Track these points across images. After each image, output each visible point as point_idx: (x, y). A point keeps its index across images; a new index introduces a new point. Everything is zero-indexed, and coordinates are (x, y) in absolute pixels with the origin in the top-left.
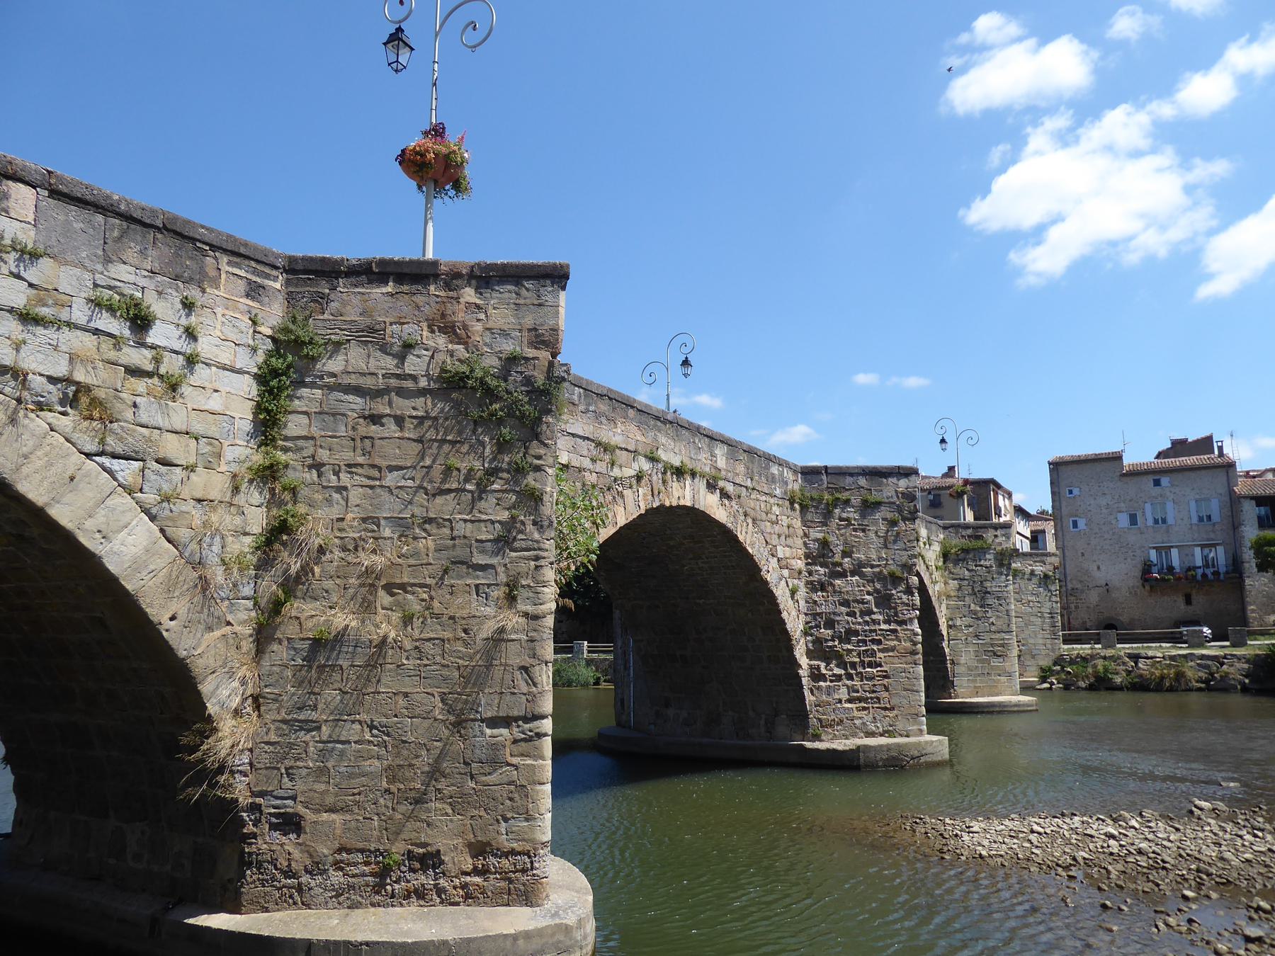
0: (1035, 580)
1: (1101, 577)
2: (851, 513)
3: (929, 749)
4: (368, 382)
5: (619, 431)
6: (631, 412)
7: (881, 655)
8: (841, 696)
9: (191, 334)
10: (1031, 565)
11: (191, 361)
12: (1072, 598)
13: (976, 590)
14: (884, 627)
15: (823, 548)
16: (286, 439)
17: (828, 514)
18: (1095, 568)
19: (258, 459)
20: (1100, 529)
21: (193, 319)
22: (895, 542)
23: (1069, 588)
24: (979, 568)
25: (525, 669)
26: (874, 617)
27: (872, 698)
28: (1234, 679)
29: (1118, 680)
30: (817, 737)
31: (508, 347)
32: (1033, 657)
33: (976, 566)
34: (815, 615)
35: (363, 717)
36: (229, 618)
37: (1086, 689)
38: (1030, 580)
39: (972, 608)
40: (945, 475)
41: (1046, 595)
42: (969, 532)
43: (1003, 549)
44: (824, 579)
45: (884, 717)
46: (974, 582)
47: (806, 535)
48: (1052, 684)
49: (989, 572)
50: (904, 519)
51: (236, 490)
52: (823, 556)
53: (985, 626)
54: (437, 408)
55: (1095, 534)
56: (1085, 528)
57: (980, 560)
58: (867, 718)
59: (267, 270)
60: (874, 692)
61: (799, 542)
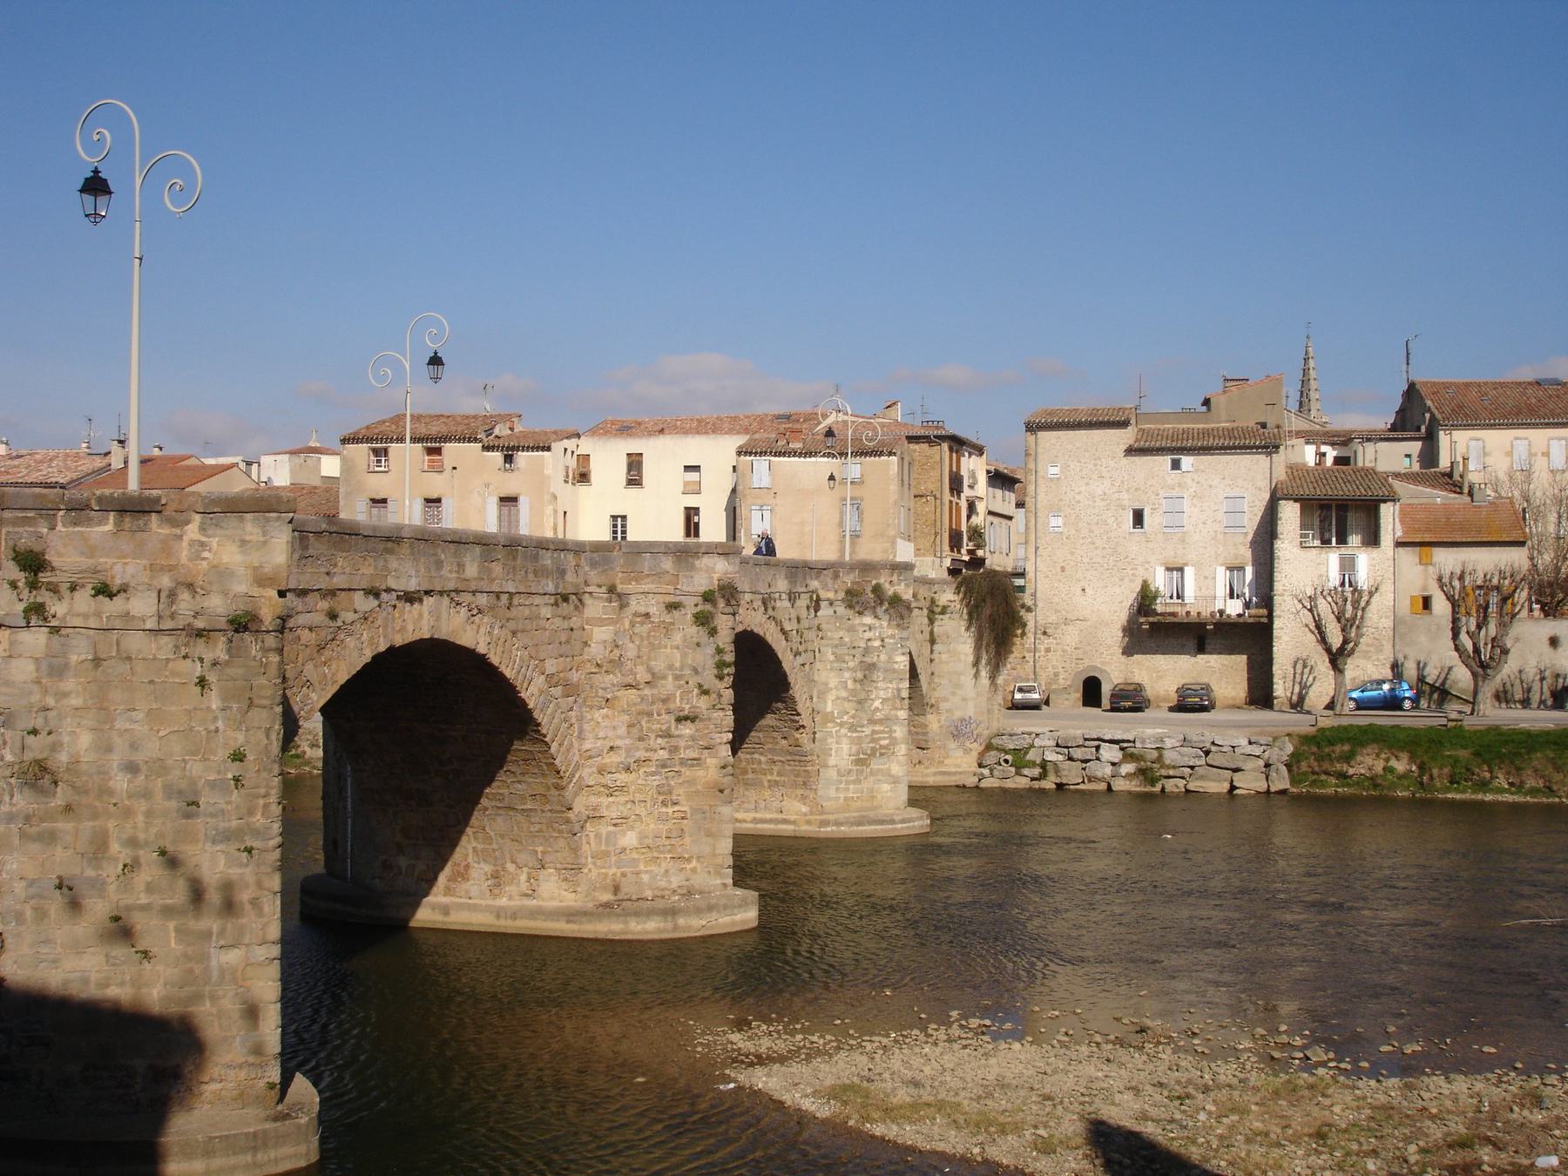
18: (1079, 591)
20: (1091, 531)
55: (1083, 538)
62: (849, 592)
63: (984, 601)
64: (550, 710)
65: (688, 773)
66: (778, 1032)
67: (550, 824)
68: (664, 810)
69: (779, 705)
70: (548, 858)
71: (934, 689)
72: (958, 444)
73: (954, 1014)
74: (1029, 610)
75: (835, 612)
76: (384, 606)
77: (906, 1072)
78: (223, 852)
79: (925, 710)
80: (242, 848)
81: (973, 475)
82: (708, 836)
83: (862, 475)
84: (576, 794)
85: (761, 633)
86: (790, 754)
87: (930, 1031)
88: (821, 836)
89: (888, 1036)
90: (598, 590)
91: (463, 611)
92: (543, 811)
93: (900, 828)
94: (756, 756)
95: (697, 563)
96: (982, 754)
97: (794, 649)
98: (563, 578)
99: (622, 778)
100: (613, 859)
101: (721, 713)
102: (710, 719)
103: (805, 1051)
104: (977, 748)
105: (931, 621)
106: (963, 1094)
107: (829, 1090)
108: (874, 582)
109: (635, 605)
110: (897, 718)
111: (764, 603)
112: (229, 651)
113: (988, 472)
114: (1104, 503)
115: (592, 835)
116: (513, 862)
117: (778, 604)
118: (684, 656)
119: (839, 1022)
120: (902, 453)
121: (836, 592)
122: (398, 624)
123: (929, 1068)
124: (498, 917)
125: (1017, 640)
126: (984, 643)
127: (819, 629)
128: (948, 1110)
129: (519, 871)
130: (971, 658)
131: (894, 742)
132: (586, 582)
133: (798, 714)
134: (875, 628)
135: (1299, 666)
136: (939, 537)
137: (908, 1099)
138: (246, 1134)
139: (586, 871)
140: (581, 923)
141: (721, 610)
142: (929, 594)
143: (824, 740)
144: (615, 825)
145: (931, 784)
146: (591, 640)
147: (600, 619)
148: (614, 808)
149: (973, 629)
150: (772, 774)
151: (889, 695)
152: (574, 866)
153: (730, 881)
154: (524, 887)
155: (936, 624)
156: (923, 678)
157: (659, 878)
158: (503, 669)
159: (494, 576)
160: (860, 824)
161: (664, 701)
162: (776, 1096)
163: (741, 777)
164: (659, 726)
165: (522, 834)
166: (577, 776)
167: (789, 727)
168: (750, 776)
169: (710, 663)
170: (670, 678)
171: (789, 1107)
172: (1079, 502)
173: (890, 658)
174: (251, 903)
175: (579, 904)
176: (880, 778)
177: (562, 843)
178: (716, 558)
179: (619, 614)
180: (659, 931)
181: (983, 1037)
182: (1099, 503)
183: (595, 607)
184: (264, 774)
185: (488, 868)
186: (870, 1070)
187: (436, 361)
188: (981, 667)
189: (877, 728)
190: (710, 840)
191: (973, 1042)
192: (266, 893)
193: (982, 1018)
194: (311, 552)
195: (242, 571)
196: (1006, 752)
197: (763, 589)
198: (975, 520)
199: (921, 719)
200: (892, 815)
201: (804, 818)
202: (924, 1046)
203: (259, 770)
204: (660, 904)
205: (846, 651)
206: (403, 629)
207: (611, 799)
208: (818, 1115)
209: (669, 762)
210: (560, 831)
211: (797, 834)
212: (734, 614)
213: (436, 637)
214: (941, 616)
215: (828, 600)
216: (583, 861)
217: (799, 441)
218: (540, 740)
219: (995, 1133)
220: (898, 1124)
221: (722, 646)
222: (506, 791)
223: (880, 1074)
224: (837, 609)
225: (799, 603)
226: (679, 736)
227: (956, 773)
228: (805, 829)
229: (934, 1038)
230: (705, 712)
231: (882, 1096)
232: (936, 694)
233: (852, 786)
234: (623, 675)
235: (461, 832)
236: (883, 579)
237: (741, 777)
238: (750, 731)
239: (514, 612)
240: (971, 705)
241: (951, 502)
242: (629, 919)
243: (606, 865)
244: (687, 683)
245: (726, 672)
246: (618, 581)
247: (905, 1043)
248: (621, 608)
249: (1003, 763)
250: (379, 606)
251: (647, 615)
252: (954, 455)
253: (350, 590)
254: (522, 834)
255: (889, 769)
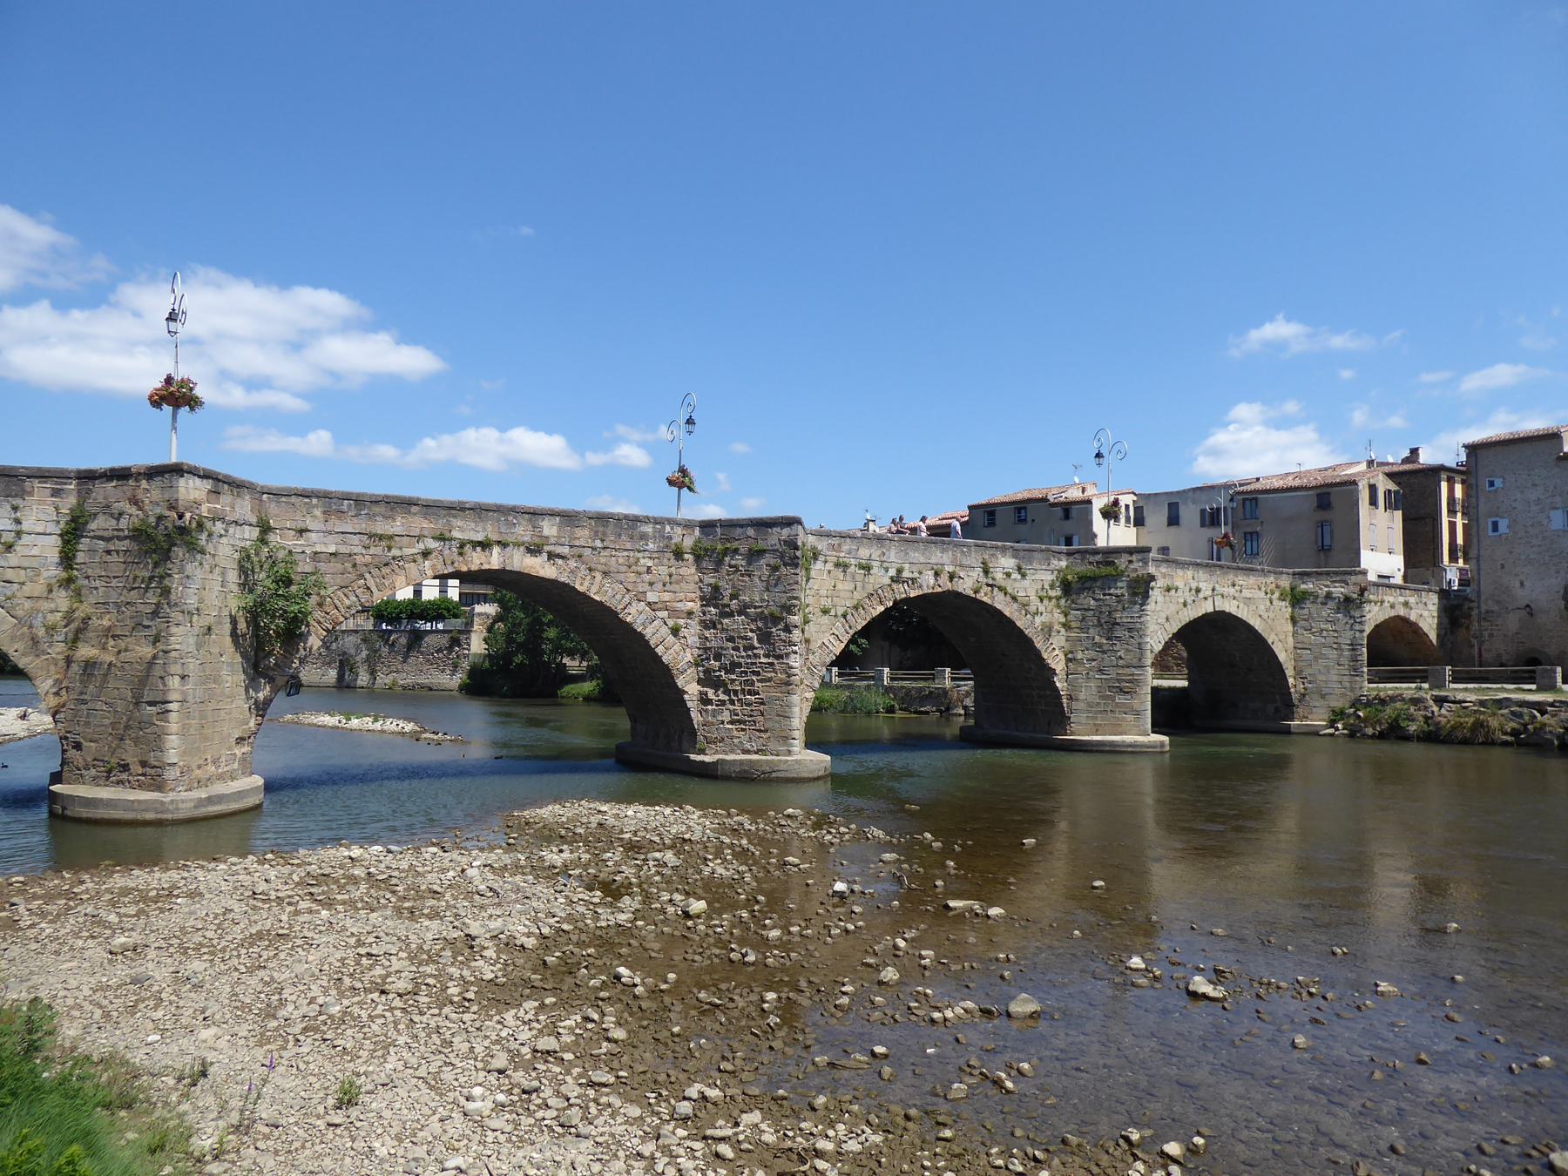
0: (1331, 604)
1: (1523, 596)
2: (739, 561)
3: (783, 767)
4: (105, 534)
5: (399, 524)
6: (414, 509)
7: (760, 685)
8: (724, 719)
9: (18, 522)
10: (1326, 586)
11: (19, 534)
12: (1486, 624)
13: (1103, 621)
14: (763, 660)
15: (716, 592)
16: (77, 564)
17: (720, 563)
18: (1518, 584)
19: (65, 575)
20: (1526, 532)
21: (18, 514)
22: (776, 585)
23: (1483, 610)
24: (1108, 597)
25: (162, 678)
26: (755, 651)
27: (749, 721)
28: (1551, 732)
29: (1413, 728)
30: (702, 752)
31: (158, 511)
32: (1323, 696)
33: (1104, 595)
34: (706, 649)
35: (103, 699)
36: (49, 651)
37: (1373, 737)
38: (1326, 604)
39: (1096, 641)
40: (1406, 461)
41: (1347, 623)
42: (1099, 558)
43: (1138, 576)
44: (714, 618)
45: (759, 737)
46: (1101, 612)
47: (701, 581)
48: (1337, 729)
49: (1119, 602)
50: (785, 565)
51: (51, 591)
52: (716, 598)
53: (1111, 661)
54: (134, 546)
55: (1521, 538)
56: (1507, 531)
57: (1110, 589)
58: (744, 737)
59: (64, 481)
60: (751, 716)
61: (692, 586)
114: (1539, 507)
135: (1255, 551)
172: (1515, 508)
182: (1534, 508)
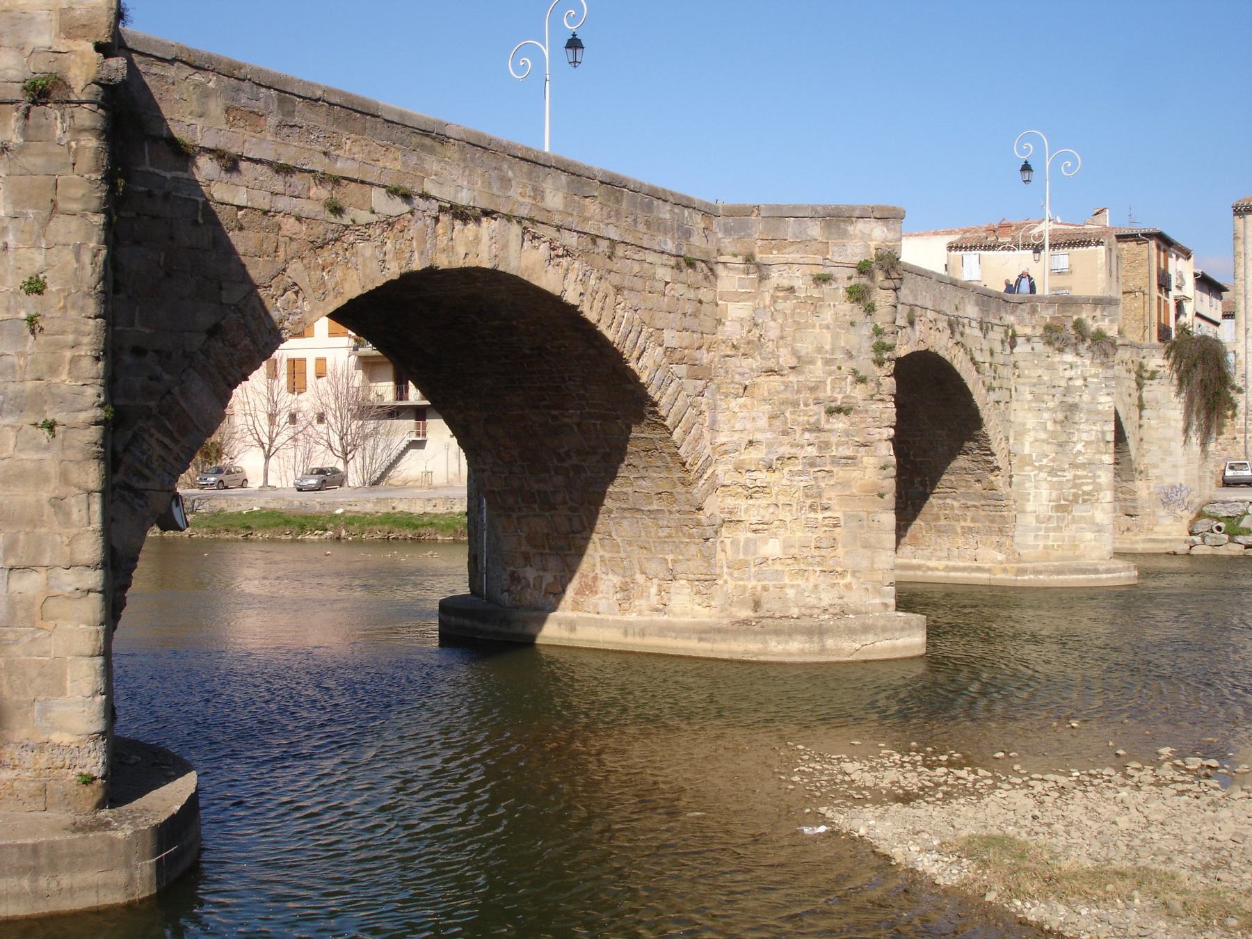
62: (1048, 328)
63: (1195, 365)
64: (670, 390)
65: (841, 473)
66: (914, 764)
67: (679, 528)
68: (812, 515)
69: (972, 444)
70: (679, 568)
71: (1143, 455)
72: (1165, 242)
73: (1165, 751)
74: (1240, 391)
75: (1033, 349)
76: (419, 214)
77: (1090, 823)
78: (13, 427)
79: (1133, 475)
80: (41, 423)
81: (1181, 276)
82: (864, 547)
83: (1070, 265)
84: (707, 493)
85: (948, 358)
86: (985, 498)
87: (1129, 771)
88: (1019, 584)
89: (1068, 774)
90: (734, 260)
91: (544, 247)
92: (671, 512)
93: (1105, 579)
94: (948, 501)
95: (850, 229)
96: (1192, 522)
97: (987, 383)
98: (687, 239)
99: (763, 477)
100: (753, 570)
101: (881, 405)
102: (867, 411)
103: (944, 788)
104: (1188, 515)
105: (1140, 386)
106: (1179, 859)
107: (962, 843)
108: (1075, 317)
109: (777, 277)
110: (1101, 463)
111: (950, 325)
112: (24, 131)
113: (1196, 275)
115: (728, 541)
116: (643, 573)
117: (967, 330)
118: (836, 337)
119: (1001, 754)
120: (1109, 244)
121: (1034, 327)
122: (443, 241)
123: (1125, 818)
124: (626, 633)
125: (1228, 422)
126: (1195, 409)
127: (1015, 366)
128: (1155, 885)
129: (649, 584)
130: (1181, 425)
131: (1098, 488)
132: (718, 250)
133: (992, 454)
134: (1077, 366)
136: (1147, 331)
137: (1089, 864)
138: (20, 846)
139: (720, 582)
140: (715, 641)
141: (879, 284)
142: (1138, 359)
143: (1021, 484)
144: (755, 531)
145: (1140, 551)
146: (726, 318)
147: (735, 293)
148: (753, 511)
149: (1183, 395)
150: (965, 520)
151: (1093, 438)
152: (708, 577)
153: (892, 602)
154: (654, 600)
155: (1145, 389)
156: (1132, 442)
157: (806, 594)
158: (602, 327)
159: (588, 214)
160: (1060, 572)
161: (813, 389)
162: (883, 848)
163: (932, 524)
164: (806, 418)
165: (651, 540)
166: (709, 472)
167: (983, 469)
168: (943, 522)
169: (867, 345)
170: (819, 363)
171: (899, 865)
173: (1093, 398)
174: (53, 506)
175: (714, 620)
176: (1084, 525)
177: (693, 549)
178: (873, 223)
179: (759, 286)
180: (802, 652)
181: (1207, 781)
183: (730, 280)
184: (73, 313)
185: (616, 580)
186: (1035, 817)
187: (574, 43)
188: (1191, 433)
189: (1080, 473)
190: (868, 553)
191: (1194, 787)
192: (76, 490)
193: (1204, 758)
194: (297, 120)
195: (43, 16)
196: (1219, 520)
197: (950, 311)
198: (1182, 319)
199: (1130, 485)
200: (1096, 564)
201: (999, 566)
202: (1119, 789)
203: (64, 307)
204: (806, 622)
205: (1045, 390)
206: (447, 250)
207: (750, 502)
208: (940, 881)
209: (818, 460)
210: (691, 536)
211: (993, 583)
212: (895, 290)
213: (501, 268)
214: (1150, 382)
215: (1025, 335)
216: (718, 571)
217: (1008, 236)
218: (659, 424)
219: (1236, 929)
220: (1068, 904)
221: (881, 327)
222: (630, 490)
223: (1049, 825)
224: (1035, 345)
225: (991, 335)
226: (830, 431)
227: (1163, 541)
228: (1001, 578)
229: (1136, 779)
230: (861, 403)
231: (1046, 857)
232: (1146, 460)
233: (1052, 534)
234: (763, 358)
235: (587, 539)
236: (1085, 315)
237: (932, 524)
238: (941, 474)
239: (617, 265)
240: (1182, 471)
241: (1159, 298)
242: (767, 637)
243: (745, 577)
244: (840, 368)
245: (886, 356)
246: (757, 250)
247: (1092, 785)
248: (760, 281)
249: (1215, 530)
250: (412, 213)
251: (791, 289)
252: (1162, 254)
253: (363, 182)
254: (651, 540)
255: (1093, 517)
